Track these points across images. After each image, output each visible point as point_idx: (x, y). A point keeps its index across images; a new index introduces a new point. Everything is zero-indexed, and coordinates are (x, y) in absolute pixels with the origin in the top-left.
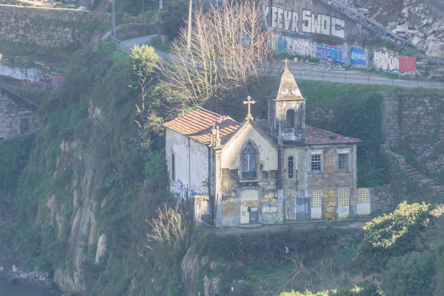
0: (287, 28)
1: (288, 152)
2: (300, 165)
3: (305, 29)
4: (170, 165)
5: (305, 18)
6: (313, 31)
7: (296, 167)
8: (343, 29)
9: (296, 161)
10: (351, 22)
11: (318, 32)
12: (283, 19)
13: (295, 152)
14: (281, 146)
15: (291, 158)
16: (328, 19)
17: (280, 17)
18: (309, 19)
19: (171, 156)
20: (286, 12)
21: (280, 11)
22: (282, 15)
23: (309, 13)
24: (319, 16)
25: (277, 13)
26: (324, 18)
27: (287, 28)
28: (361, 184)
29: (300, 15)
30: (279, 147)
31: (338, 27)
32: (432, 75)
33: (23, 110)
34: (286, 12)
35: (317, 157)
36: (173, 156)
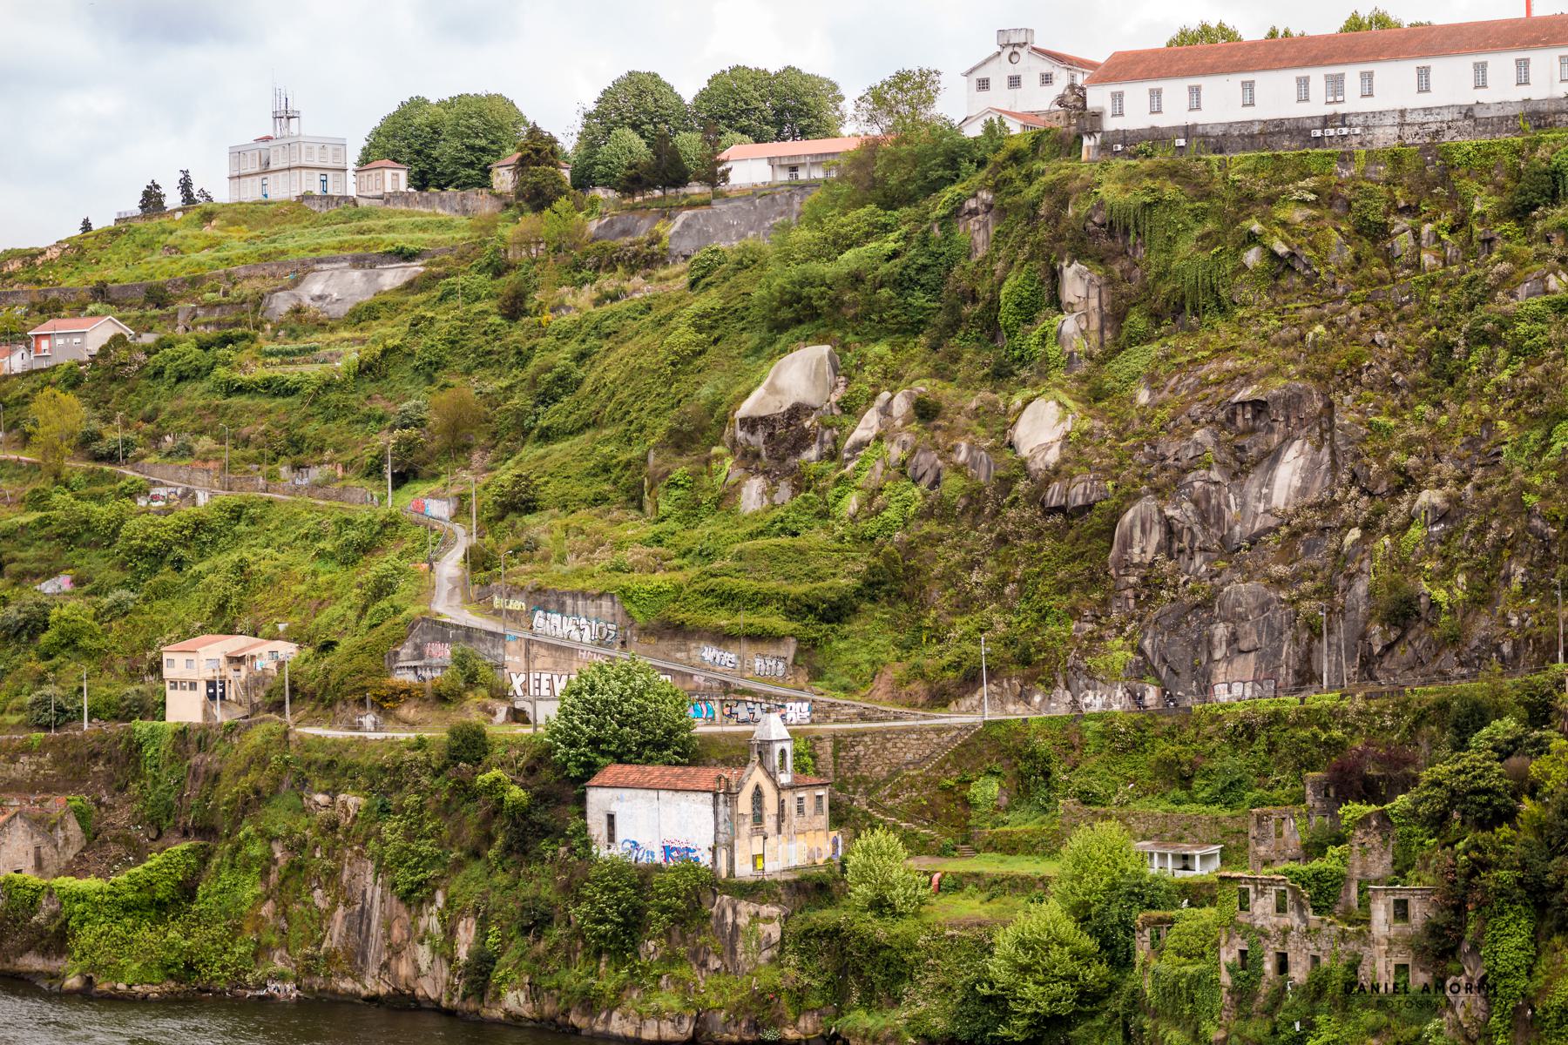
14: (780, 789)
17: (545, 684)
19: (604, 819)
20: (556, 678)
32: (833, 716)
35: (800, 799)
36: (611, 818)
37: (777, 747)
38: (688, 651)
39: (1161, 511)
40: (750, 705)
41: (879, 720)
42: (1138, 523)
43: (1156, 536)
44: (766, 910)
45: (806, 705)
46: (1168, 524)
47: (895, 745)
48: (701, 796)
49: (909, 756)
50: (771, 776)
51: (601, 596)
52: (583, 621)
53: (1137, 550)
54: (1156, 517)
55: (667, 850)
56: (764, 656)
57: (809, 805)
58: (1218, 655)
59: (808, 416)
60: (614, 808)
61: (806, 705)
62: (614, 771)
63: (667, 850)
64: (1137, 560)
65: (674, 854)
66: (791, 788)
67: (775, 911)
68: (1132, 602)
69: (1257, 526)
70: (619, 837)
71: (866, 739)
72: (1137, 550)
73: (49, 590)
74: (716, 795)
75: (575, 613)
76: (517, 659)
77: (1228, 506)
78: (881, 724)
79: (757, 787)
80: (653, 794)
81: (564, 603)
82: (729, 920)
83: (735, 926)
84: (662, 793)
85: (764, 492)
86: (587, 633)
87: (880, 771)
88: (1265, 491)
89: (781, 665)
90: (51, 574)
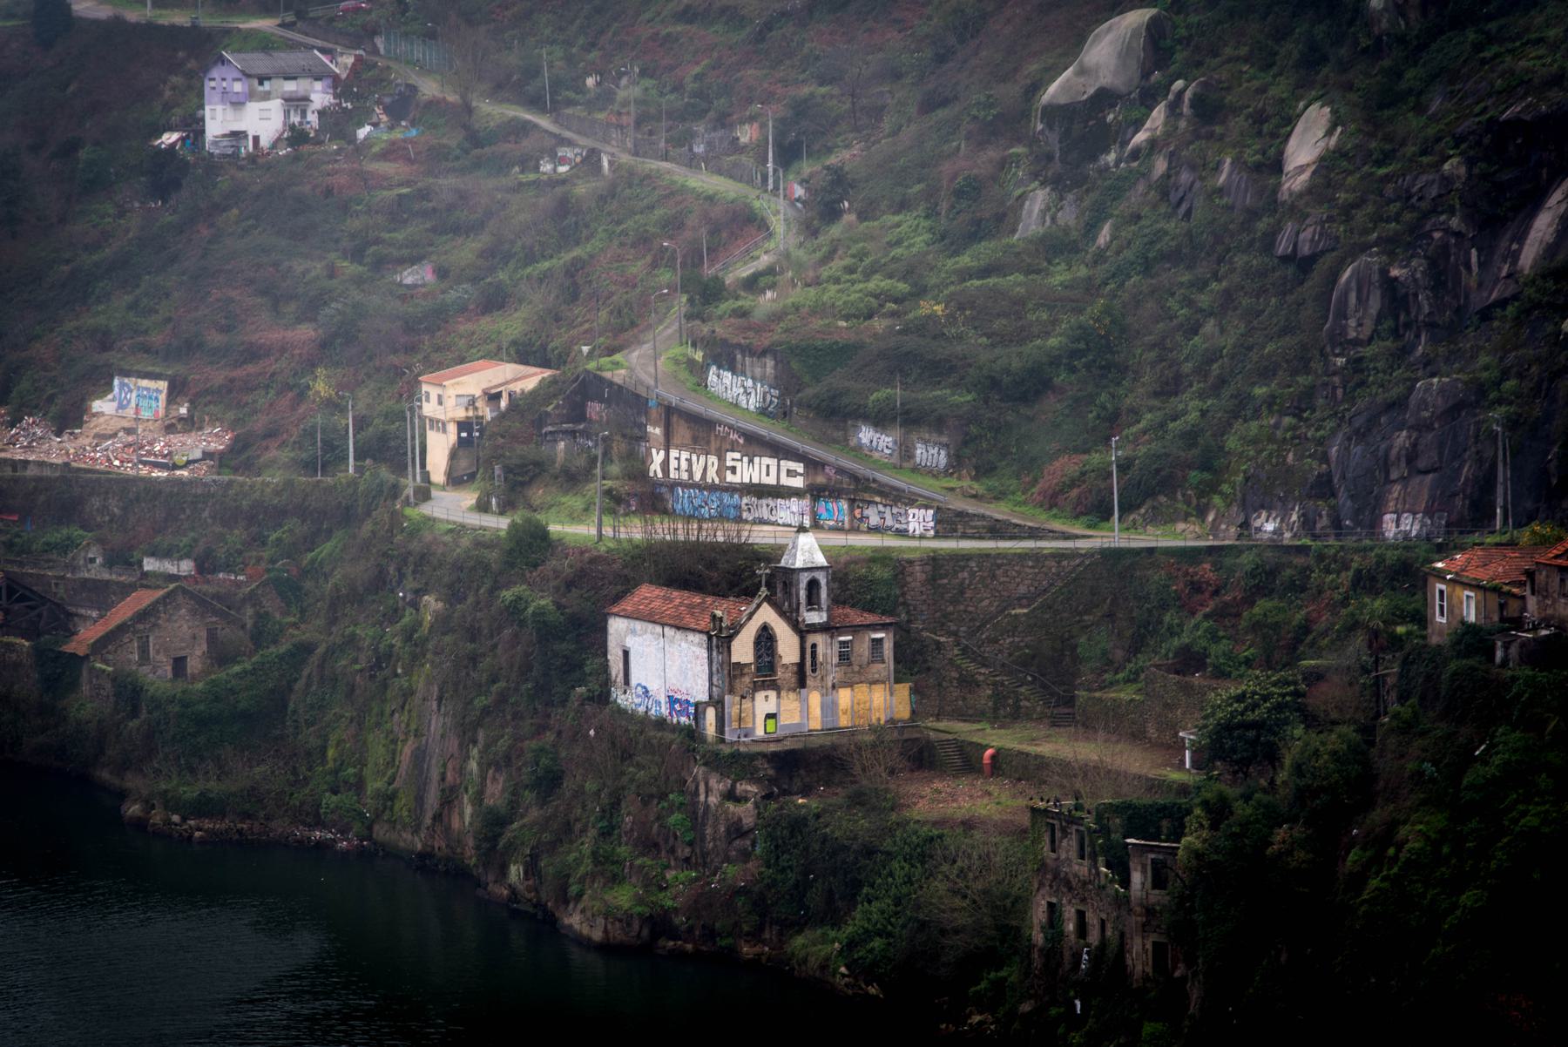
0: (697, 477)
1: (812, 638)
2: (825, 655)
3: (730, 478)
4: (1175, 535)
5: (729, 463)
6: (746, 480)
7: (820, 658)
9: (820, 650)
10: (813, 465)
11: (755, 480)
12: (690, 465)
13: (819, 639)
14: (802, 631)
15: (814, 646)
16: (773, 462)
17: (684, 465)
18: (738, 464)
19: (621, 653)
20: (694, 457)
21: (685, 455)
22: (689, 460)
23: (737, 455)
24: (757, 460)
25: (678, 459)
26: (766, 461)
27: (697, 477)
28: (897, 681)
29: (721, 459)
31: (790, 473)
33: (874, 481)
34: (694, 457)
36: (626, 654)
37: (804, 579)
38: (845, 430)
39: (1384, 272)
40: (881, 508)
41: (1012, 538)
42: (1353, 284)
43: (1375, 304)
44: (744, 787)
45: (931, 512)
46: (1390, 285)
47: (1005, 574)
48: (692, 637)
49: (1022, 590)
51: (764, 353)
52: (750, 383)
53: (1352, 323)
54: (1376, 277)
55: (672, 701)
56: (926, 442)
57: (863, 649)
58: (1394, 475)
59: (1113, 106)
60: (630, 642)
61: (931, 512)
62: (648, 594)
63: (672, 701)
64: (1352, 334)
65: (677, 707)
66: (823, 629)
67: (752, 788)
68: (1340, 392)
69: (1494, 296)
70: (634, 682)
71: (973, 564)
72: (1352, 323)
73: (409, 280)
74: (710, 638)
75: (743, 373)
76: (658, 431)
77: (1468, 267)
78: (1069, 544)
80: (658, 629)
81: (734, 359)
82: (702, 798)
83: (707, 807)
84: (667, 629)
85: (1048, 209)
86: (752, 400)
87: (986, 604)
88: (1515, 246)
89: (943, 453)
90: (414, 260)
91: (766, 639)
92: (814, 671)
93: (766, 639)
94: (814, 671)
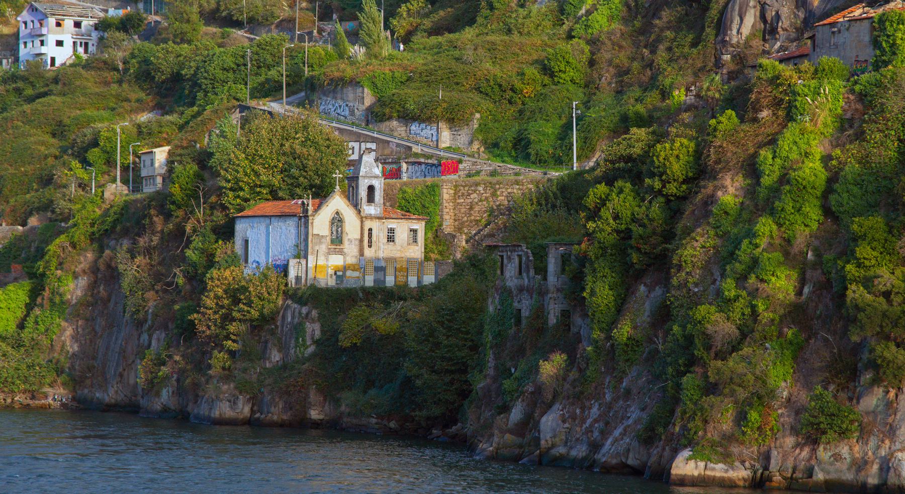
1: (368, 224)
7: (374, 238)
8: (374, 151)
30: (362, 218)
35: (391, 231)
36: (247, 242)
50: (356, 205)
79: (337, 213)
91: (337, 221)
92: (370, 246)
93: (337, 221)
94: (370, 246)
